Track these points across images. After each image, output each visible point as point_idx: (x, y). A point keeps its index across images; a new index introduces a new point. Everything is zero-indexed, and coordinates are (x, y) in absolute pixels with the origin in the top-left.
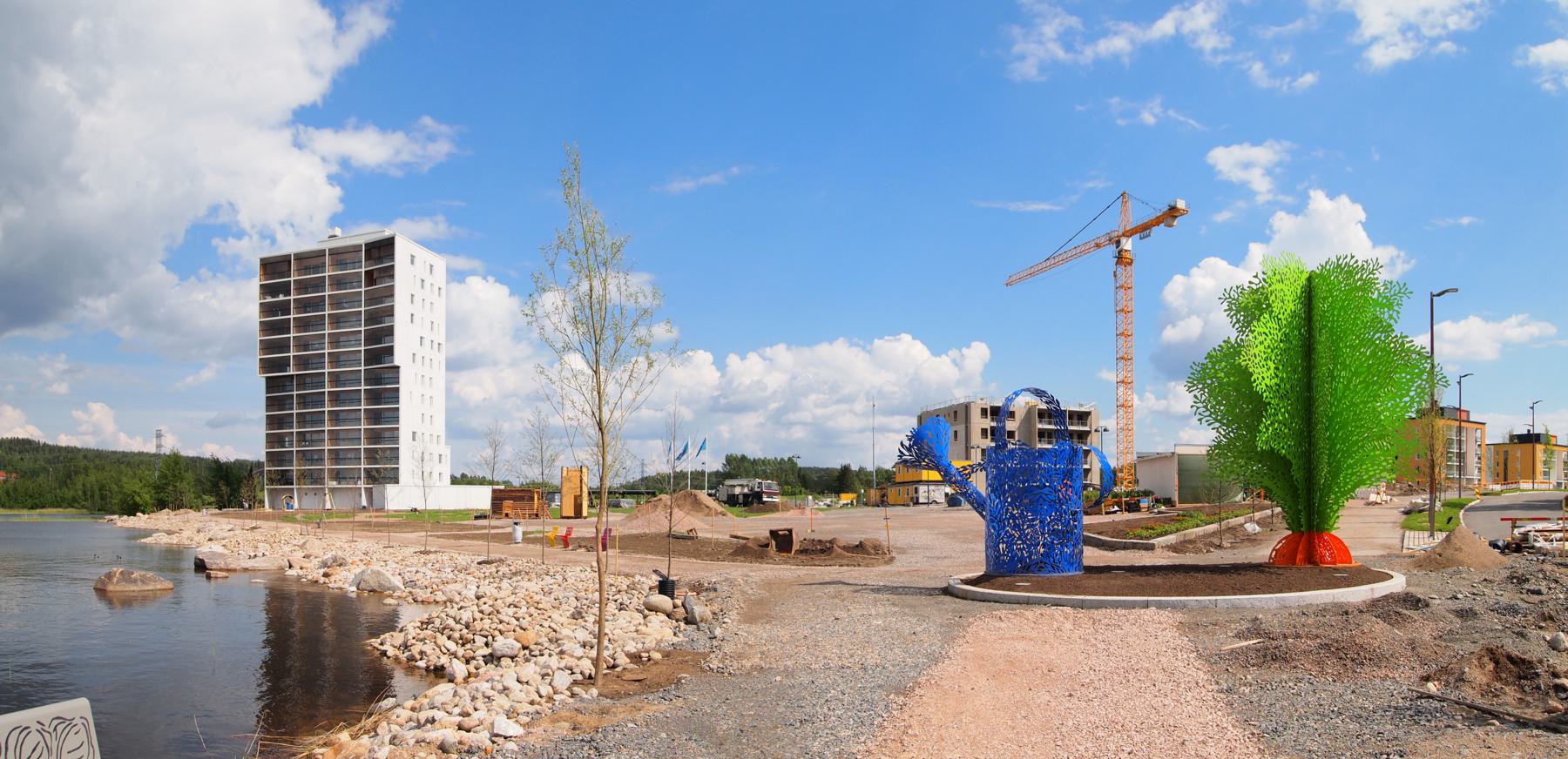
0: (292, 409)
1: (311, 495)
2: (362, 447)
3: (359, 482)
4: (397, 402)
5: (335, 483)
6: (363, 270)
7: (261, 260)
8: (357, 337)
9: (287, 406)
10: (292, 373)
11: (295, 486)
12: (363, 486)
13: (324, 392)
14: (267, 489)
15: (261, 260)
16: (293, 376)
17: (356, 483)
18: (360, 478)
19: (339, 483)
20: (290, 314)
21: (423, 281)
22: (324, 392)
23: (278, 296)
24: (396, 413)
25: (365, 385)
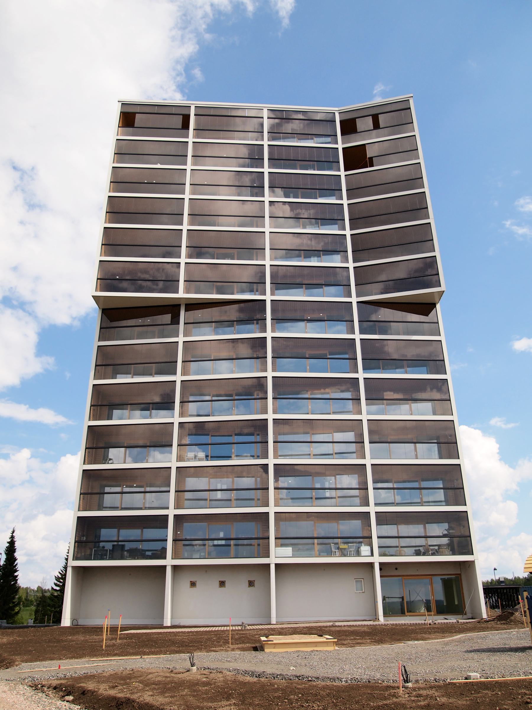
3: (365, 549)
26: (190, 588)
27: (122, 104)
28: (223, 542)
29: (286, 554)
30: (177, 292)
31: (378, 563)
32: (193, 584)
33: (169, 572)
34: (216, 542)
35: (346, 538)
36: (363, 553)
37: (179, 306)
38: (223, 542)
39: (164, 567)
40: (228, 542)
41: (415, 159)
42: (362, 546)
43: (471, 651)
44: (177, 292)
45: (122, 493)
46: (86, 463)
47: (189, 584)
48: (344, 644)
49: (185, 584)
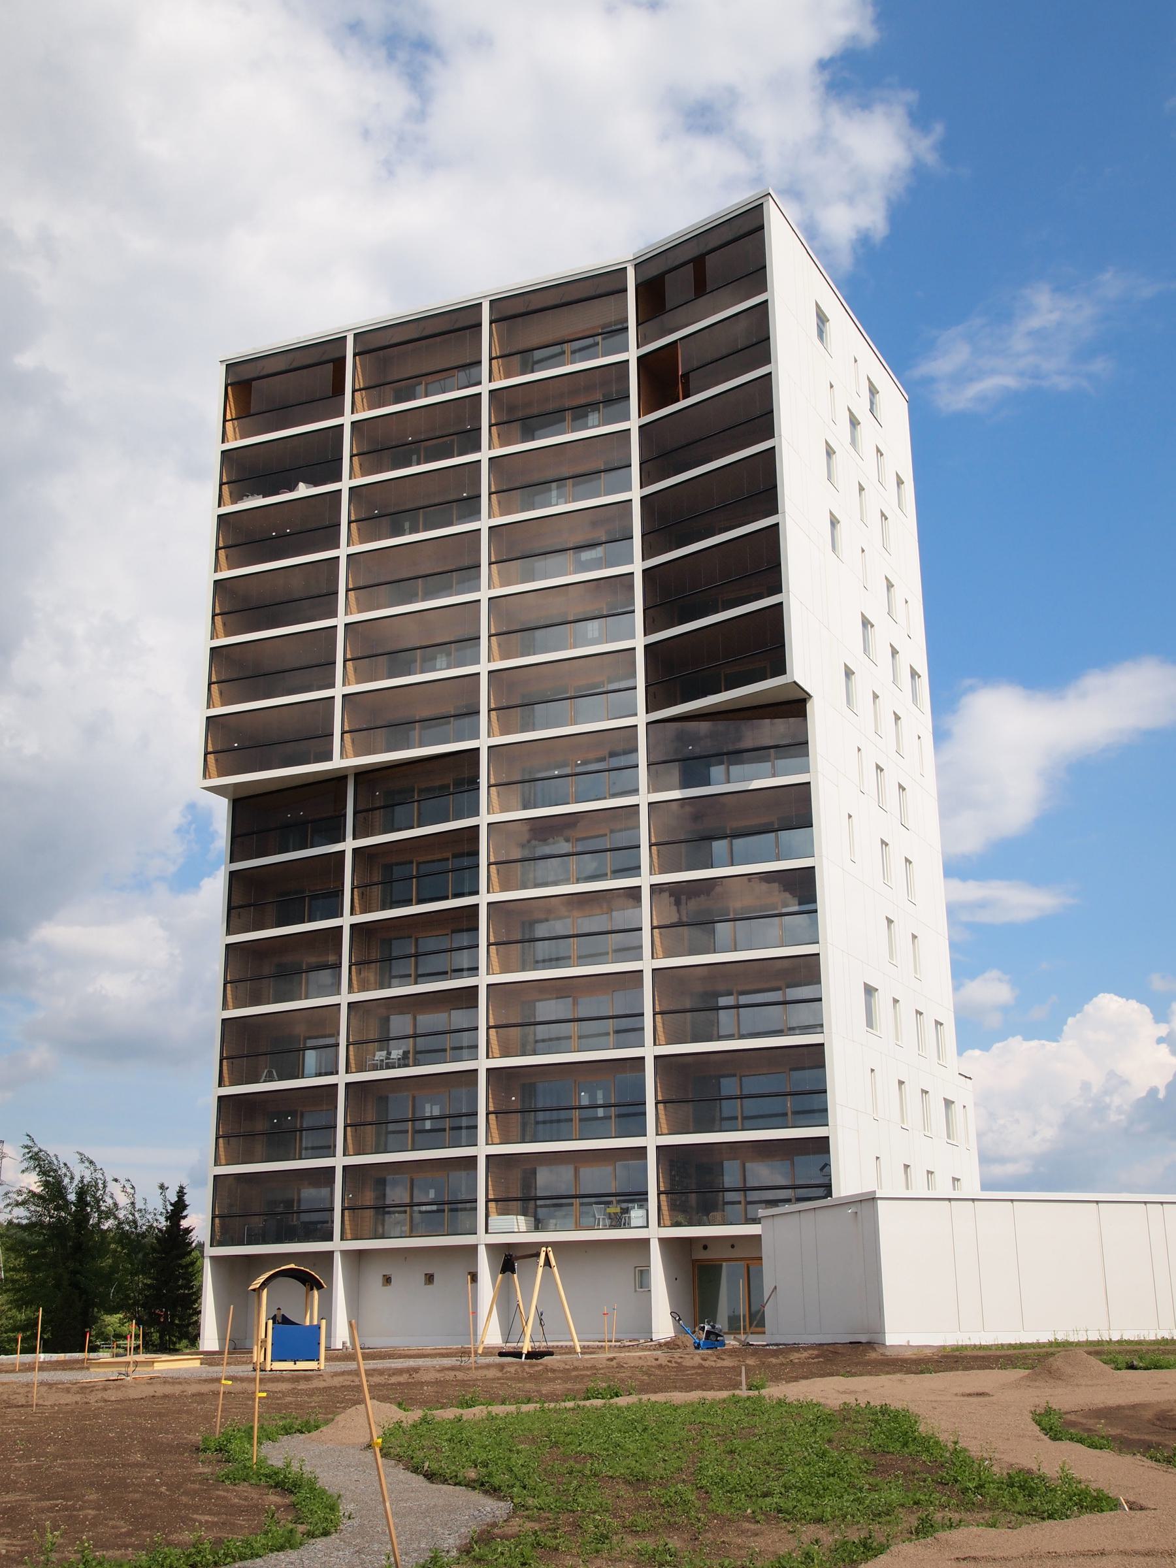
0: (329, 1150)
1: (408, 1281)
2: (649, 1051)
3: (636, 1215)
4: (820, 1114)
5: (521, 1222)
6: (632, 355)
7: (231, 367)
8: (621, 918)
9: (308, 1140)
10: (337, 763)
11: (337, 1245)
12: (655, 1233)
13: (473, 1159)
14: (214, 1259)
15: (231, 367)
16: (337, 780)
17: (618, 1221)
18: (640, 1197)
19: (538, 1226)
20: (332, 686)
21: (890, 921)
22: (473, 1159)
23: (292, 488)
24: (802, 1078)
25: (654, 787)
26: (425, 1284)
27: (227, 365)
28: (434, 1208)
29: (501, 1227)
30: (328, 757)
31: (657, 1239)
32: (387, 1280)
33: (338, 1260)
34: (424, 1208)
35: (601, 1198)
36: (634, 1223)
37: (345, 777)
38: (434, 1208)
39: (330, 1254)
40: (441, 1207)
41: (605, 495)
42: (634, 1208)
43: (970, 1395)
44: (328, 757)
45: (738, 1007)
46: (227, 1083)
47: (380, 1280)
48: (75, 1369)
49: (373, 1280)
